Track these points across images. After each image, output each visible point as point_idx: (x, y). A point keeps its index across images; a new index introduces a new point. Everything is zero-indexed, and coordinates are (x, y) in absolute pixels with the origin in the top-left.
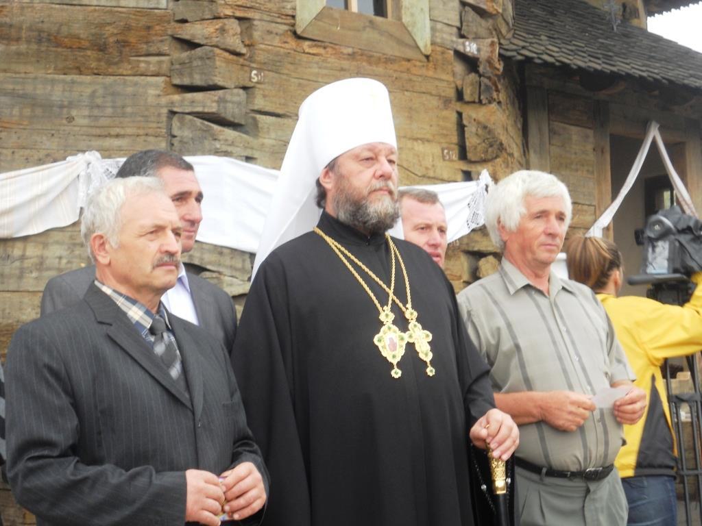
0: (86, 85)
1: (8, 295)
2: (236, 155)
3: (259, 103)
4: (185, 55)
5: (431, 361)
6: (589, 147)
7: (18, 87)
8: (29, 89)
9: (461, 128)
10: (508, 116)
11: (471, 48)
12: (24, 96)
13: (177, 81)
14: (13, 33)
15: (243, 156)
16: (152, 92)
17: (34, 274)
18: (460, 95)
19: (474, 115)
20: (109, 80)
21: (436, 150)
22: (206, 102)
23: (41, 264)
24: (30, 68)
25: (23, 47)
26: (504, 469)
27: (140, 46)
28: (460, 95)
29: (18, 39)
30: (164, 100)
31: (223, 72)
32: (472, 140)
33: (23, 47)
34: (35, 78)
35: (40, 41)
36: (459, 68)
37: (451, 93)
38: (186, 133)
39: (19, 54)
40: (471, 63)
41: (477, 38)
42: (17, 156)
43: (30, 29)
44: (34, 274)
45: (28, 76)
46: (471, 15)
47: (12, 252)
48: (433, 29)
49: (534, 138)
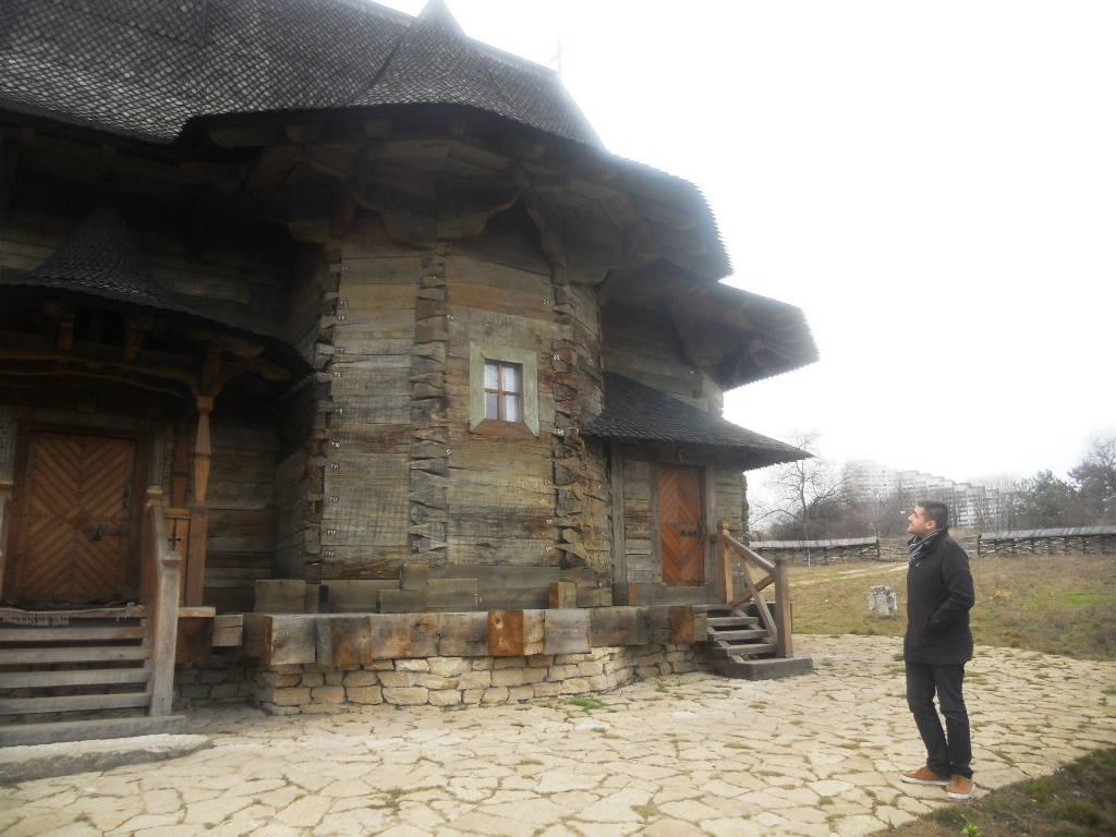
0: (375, 458)
3: (451, 463)
4: (417, 444)
6: (647, 471)
8: (353, 460)
9: (554, 469)
11: (561, 432)
13: (413, 455)
16: (404, 460)
18: (553, 455)
19: (561, 463)
20: (385, 455)
21: (541, 480)
22: (426, 464)
25: (350, 442)
26: (75, 777)
27: (161, 492)
28: (553, 455)
30: (408, 464)
31: (433, 451)
32: (559, 475)
33: (350, 442)
36: (555, 441)
37: (549, 453)
38: (417, 478)
40: (561, 439)
41: (564, 428)
46: (561, 417)
48: (540, 425)
49: (614, 468)
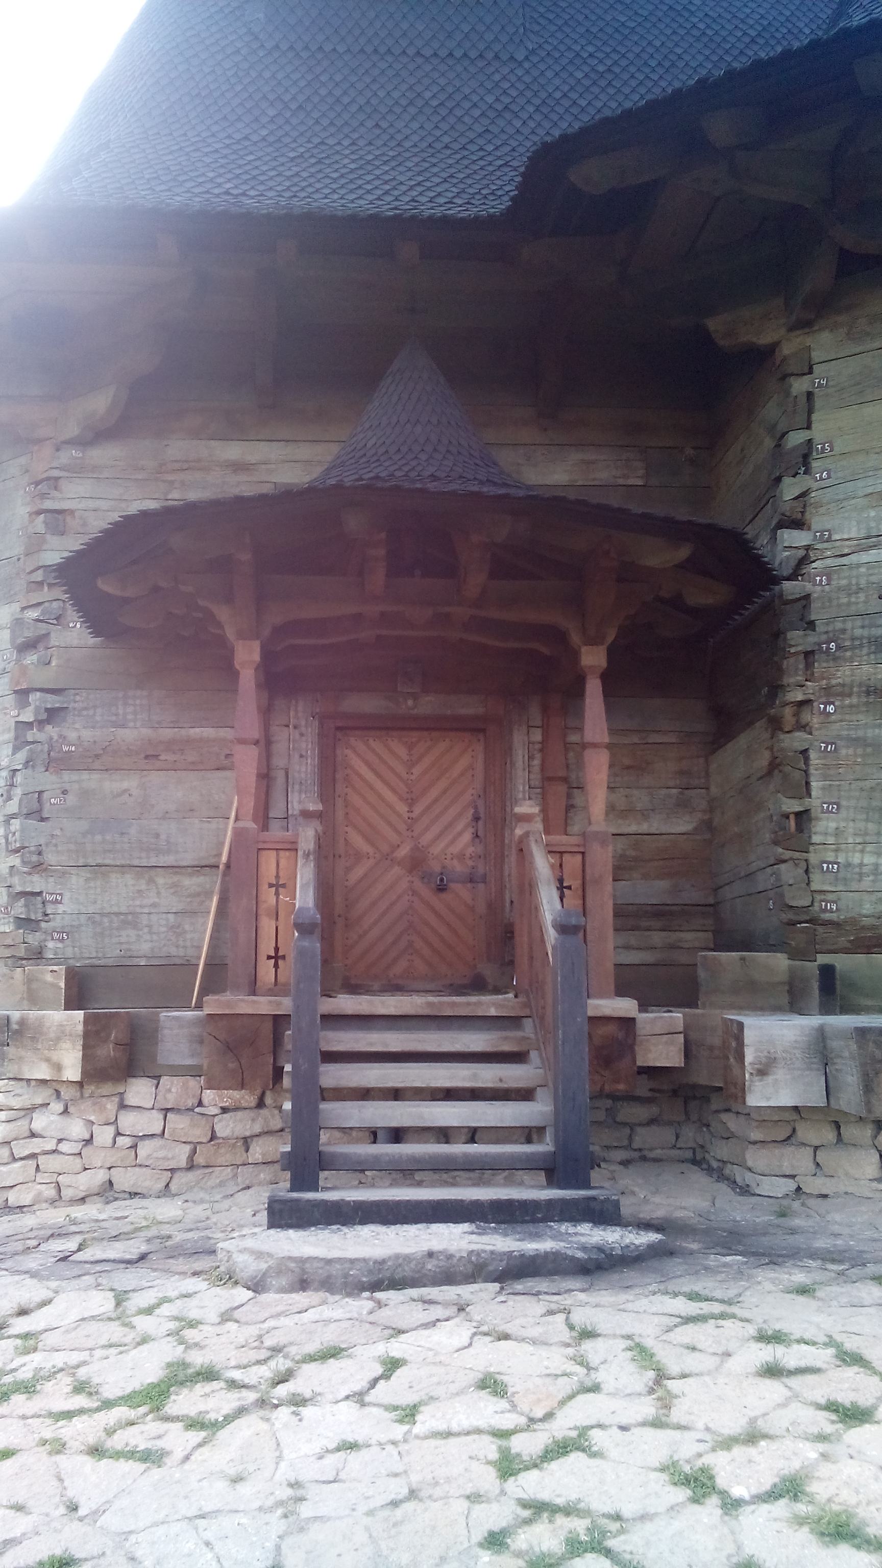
1: (851, 894)
2: (330, 1397)
5: (602, 644)
7: (852, 732)
10: (742, 1427)
12: (857, 739)
14: (847, 690)
15: (460, 1496)
17: (871, 878)
23: (876, 869)
24: (860, 717)
25: (855, 700)
29: (850, 695)
33: (855, 700)
34: (866, 724)
35: (868, 693)
39: (851, 706)
42: (853, 786)
43: (860, 685)
44: (871, 878)
45: (860, 723)
47: (853, 857)
